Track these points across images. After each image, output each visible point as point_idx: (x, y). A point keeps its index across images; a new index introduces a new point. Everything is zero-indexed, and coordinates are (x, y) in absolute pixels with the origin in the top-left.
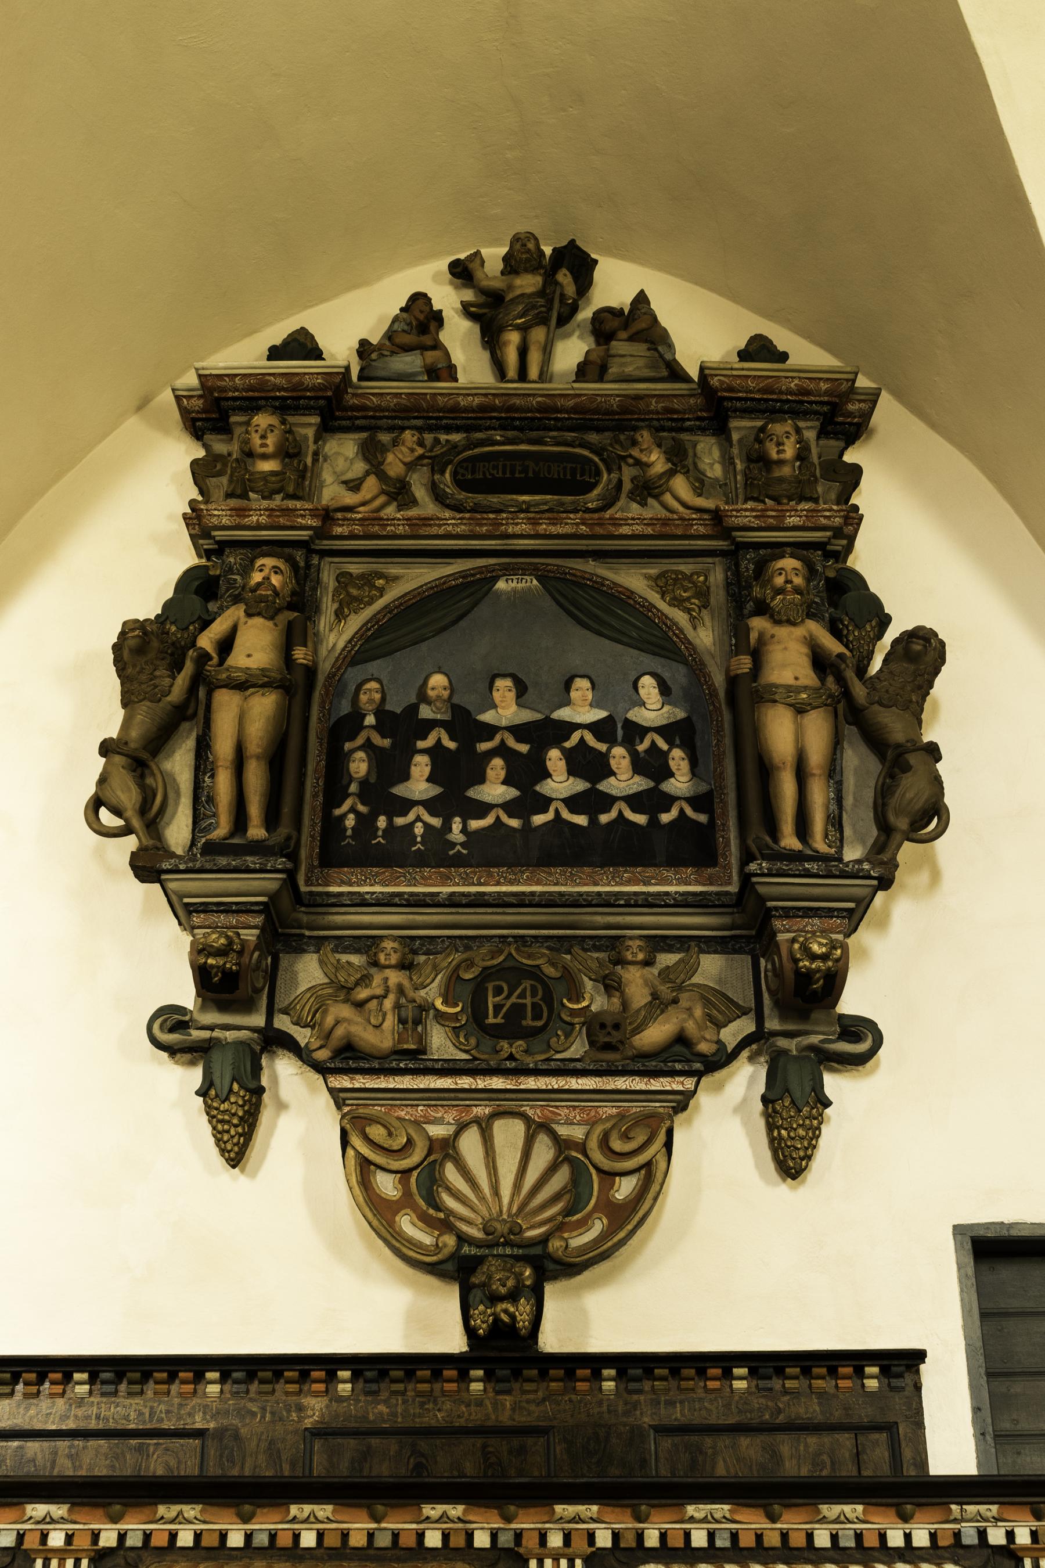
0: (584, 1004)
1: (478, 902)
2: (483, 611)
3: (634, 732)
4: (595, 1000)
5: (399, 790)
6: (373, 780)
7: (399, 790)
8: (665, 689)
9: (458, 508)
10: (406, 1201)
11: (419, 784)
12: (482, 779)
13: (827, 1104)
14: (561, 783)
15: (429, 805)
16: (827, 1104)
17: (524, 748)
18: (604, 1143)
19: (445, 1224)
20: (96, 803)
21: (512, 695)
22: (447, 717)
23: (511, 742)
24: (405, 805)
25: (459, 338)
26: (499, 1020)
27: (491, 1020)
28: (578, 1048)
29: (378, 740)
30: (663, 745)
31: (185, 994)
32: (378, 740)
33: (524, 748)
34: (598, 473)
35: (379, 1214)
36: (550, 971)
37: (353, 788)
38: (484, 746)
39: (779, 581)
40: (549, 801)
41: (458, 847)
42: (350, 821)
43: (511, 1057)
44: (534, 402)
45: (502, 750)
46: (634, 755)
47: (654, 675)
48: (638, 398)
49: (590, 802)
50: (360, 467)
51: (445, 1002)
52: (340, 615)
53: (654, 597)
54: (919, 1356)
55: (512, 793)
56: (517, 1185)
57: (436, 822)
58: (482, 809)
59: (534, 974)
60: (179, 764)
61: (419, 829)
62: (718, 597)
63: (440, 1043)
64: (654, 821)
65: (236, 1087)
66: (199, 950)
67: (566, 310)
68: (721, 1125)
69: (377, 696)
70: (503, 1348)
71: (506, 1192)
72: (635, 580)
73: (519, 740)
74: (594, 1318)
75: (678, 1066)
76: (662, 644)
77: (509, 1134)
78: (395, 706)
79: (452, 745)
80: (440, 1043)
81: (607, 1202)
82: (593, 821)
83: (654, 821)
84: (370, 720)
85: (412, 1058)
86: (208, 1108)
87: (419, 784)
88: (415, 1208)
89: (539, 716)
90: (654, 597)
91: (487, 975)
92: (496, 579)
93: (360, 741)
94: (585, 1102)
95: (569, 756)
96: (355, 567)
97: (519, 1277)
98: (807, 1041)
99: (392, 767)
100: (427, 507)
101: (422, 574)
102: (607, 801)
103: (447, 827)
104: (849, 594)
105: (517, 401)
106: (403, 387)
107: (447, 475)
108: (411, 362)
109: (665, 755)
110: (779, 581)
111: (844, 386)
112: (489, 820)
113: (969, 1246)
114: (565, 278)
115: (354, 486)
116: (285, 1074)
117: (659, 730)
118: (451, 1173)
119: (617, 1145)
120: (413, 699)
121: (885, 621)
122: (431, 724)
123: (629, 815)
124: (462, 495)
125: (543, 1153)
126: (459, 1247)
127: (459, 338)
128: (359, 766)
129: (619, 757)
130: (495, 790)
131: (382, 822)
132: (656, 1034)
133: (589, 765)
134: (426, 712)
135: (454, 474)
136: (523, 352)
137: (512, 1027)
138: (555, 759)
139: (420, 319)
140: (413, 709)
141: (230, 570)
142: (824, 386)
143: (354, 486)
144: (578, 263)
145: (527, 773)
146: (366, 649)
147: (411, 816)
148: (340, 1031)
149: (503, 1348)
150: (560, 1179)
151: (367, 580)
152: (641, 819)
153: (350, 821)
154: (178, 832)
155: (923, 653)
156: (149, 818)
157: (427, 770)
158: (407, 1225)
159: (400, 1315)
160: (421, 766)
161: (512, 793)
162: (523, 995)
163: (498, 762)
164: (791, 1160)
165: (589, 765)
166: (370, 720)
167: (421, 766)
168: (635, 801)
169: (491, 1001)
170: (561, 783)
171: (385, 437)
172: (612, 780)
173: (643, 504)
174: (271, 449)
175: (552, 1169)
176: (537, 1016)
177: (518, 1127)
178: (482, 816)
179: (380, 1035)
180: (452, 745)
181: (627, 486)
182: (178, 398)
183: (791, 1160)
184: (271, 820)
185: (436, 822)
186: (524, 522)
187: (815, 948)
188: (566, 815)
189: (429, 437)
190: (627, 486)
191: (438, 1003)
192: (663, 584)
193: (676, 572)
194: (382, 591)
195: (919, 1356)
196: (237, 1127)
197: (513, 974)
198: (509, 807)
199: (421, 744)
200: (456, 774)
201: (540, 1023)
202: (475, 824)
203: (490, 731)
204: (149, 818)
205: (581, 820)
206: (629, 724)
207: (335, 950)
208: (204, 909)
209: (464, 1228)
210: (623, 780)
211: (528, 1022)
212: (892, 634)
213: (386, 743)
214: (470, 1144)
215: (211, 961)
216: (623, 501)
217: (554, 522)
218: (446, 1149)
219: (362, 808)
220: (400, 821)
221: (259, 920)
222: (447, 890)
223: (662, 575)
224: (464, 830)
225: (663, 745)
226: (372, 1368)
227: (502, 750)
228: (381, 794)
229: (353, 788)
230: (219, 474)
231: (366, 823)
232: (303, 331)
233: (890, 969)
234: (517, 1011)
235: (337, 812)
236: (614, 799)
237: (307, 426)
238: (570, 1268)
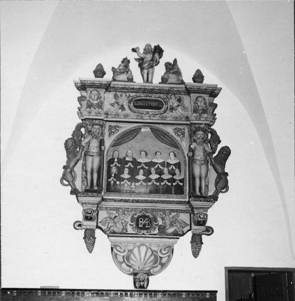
1: (138, 201)
2: (138, 136)
3: (169, 165)
4: (160, 222)
5: (122, 176)
6: (117, 173)
7: (122, 176)
8: (175, 156)
9: (134, 112)
10: (124, 262)
11: (126, 175)
12: (138, 174)
13: (203, 243)
15: (128, 179)
16: (203, 243)
17: (147, 168)
18: (161, 251)
21: (144, 156)
22: (132, 160)
23: (144, 166)
24: (123, 179)
25: (134, 66)
26: (142, 226)
27: (140, 226)
28: (156, 231)
29: (118, 165)
30: (174, 168)
31: (80, 218)
32: (118, 165)
34: (163, 105)
36: (151, 216)
37: (113, 175)
38: (138, 167)
39: (199, 136)
42: (112, 182)
44: (150, 88)
45: (143, 168)
47: (173, 152)
48: (172, 88)
49: (160, 180)
50: (113, 101)
51: (131, 222)
52: (110, 135)
53: (173, 134)
54: (216, 292)
55: (145, 178)
56: (144, 259)
59: (148, 217)
60: (78, 169)
62: (187, 134)
63: (130, 230)
64: (172, 185)
65: (91, 238)
66: (84, 210)
67: (156, 64)
69: (118, 155)
70: (141, 288)
71: (142, 260)
72: (170, 130)
73: (146, 166)
74: (156, 283)
76: (175, 145)
77: (143, 249)
78: (121, 157)
79: (132, 166)
80: (130, 230)
81: (160, 262)
82: (160, 184)
83: (172, 185)
84: (116, 160)
85: (124, 234)
86: (86, 242)
87: (126, 175)
88: (125, 263)
89: (150, 161)
90: (173, 134)
91: (139, 217)
92: (141, 128)
93: (114, 164)
94: (157, 243)
95: (156, 169)
96: (113, 124)
98: (200, 230)
99: (121, 171)
100: (127, 111)
101: (126, 127)
102: (163, 180)
105: (147, 87)
107: (132, 104)
108: (123, 77)
109: (174, 170)
110: (199, 136)
111: (215, 89)
112: (140, 183)
113: (227, 270)
114: (157, 55)
115: (112, 105)
116: (98, 232)
117: (174, 165)
118: (132, 256)
119: (163, 252)
121: (219, 142)
122: (129, 161)
123: (167, 183)
124: (135, 109)
125: (149, 253)
126: (133, 271)
127: (134, 66)
128: (114, 170)
132: (171, 230)
133: (160, 173)
134: (127, 159)
135: (133, 104)
136: (148, 74)
137: (144, 228)
140: (125, 158)
141: (87, 125)
142: (210, 88)
143: (112, 105)
144: (158, 51)
146: (117, 143)
147: (124, 182)
148: (112, 228)
149: (141, 288)
150: (153, 257)
151: (115, 127)
152: (170, 184)
154: (79, 185)
155: (226, 152)
157: (128, 172)
160: (126, 171)
161: (145, 178)
162: (146, 221)
163: (141, 171)
164: (196, 254)
165: (160, 173)
166: (116, 160)
167: (126, 171)
168: (168, 180)
169: (140, 222)
170: (154, 176)
171: (119, 94)
174: (96, 99)
175: (151, 256)
176: (149, 225)
177: (145, 248)
180: (132, 166)
181: (169, 108)
182: (75, 83)
183: (196, 254)
184: (98, 185)
186: (149, 116)
187: (201, 216)
188: (155, 183)
189: (128, 94)
190: (169, 108)
191: (130, 222)
192: (177, 131)
193: (179, 128)
195: (216, 292)
197: (144, 217)
199: (126, 166)
202: (137, 184)
203: (140, 163)
206: (168, 163)
207: (110, 210)
208: (86, 203)
209: (134, 267)
210: (166, 176)
212: (220, 147)
213: (120, 165)
214: (136, 251)
215: (88, 215)
216: (168, 111)
218: (131, 251)
220: (122, 183)
223: (176, 129)
224: (135, 185)
225: (174, 168)
227: (143, 168)
228: (118, 177)
229: (113, 175)
230: (84, 100)
233: (215, 215)
234: (145, 225)
235: (109, 180)
238: (152, 275)
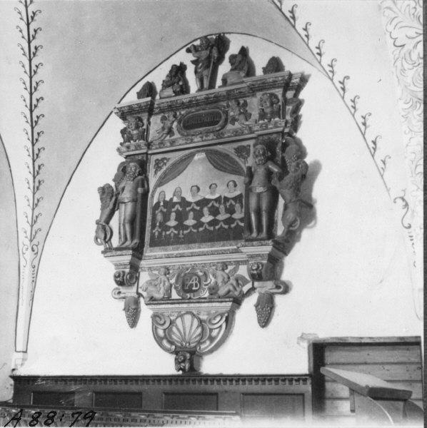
0: (208, 282)
11: (172, 223)
14: (207, 218)
15: (174, 227)
19: (171, 343)
20: (96, 238)
33: (198, 208)
35: (159, 340)
37: (158, 224)
38: (188, 209)
40: (203, 223)
41: (222, 223)
42: (157, 234)
43: (190, 298)
45: (193, 210)
46: (226, 207)
48: (230, 91)
57: (176, 232)
58: (187, 227)
61: (172, 235)
63: (175, 295)
68: (247, 312)
74: (210, 366)
75: (227, 300)
80: (175, 295)
83: (230, 228)
85: (167, 299)
87: (172, 223)
88: (167, 339)
96: (159, 157)
97: (185, 357)
99: (166, 217)
100: (177, 135)
103: (179, 234)
104: (290, 146)
106: (168, 100)
109: (234, 206)
118: (174, 329)
120: (172, 197)
123: (224, 226)
125: (196, 323)
129: (222, 208)
130: (190, 222)
131: (164, 234)
138: (206, 210)
139: (179, 71)
142: (280, 79)
145: (198, 215)
153: (157, 234)
156: (107, 239)
158: (165, 342)
159: (165, 365)
160: (173, 215)
163: (192, 213)
164: (265, 320)
167: (173, 215)
172: (220, 215)
173: (234, 124)
175: (197, 327)
178: (187, 230)
179: (159, 296)
180: (181, 209)
183: (265, 320)
185: (176, 232)
194: (165, 164)
196: (133, 317)
198: (194, 226)
199: (173, 210)
200: (181, 217)
201: (197, 288)
202: (185, 232)
204: (107, 239)
205: (212, 228)
211: (194, 288)
214: (179, 322)
217: (206, 136)
219: (160, 230)
220: (168, 233)
221: (129, 266)
222: (177, 252)
226: (158, 379)
231: (160, 234)
232: (148, 82)
236: (220, 221)
237: (145, 117)
